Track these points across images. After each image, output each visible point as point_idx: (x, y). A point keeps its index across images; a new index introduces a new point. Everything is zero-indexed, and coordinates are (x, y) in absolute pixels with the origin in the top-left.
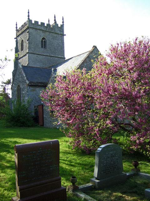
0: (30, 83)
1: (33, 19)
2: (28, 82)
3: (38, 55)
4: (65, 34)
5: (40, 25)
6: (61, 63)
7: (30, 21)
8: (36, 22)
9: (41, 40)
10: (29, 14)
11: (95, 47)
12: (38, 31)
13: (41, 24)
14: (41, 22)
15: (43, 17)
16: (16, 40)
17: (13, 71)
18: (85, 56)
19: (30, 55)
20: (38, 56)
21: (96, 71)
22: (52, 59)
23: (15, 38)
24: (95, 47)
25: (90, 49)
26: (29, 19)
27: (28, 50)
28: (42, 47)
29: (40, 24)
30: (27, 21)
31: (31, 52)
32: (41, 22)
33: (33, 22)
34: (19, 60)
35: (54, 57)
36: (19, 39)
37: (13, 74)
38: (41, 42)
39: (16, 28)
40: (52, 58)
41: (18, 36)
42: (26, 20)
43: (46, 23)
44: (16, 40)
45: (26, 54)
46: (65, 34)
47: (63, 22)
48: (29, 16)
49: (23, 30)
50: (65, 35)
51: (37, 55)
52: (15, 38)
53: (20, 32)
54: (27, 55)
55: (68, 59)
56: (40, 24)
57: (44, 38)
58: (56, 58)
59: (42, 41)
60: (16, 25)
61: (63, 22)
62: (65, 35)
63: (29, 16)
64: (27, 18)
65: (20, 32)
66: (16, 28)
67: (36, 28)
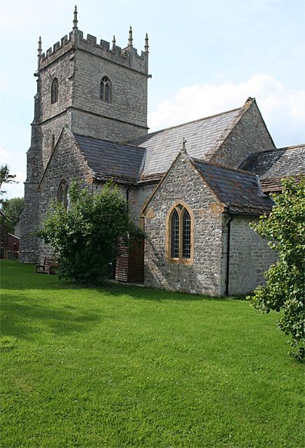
0: (97, 175)
1: (86, 29)
2: (94, 173)
3: (93, 116)
4: (149, 74)
5: (98, 46)
6: (142, 138)
7: (77, 33)
8: (92, 39)
9: (100, 82)
10: (76, 17)
11: (252, 102)
12: (95, 58)
13: (101, 43)
14: (101, 40)
15: (104, 27)
16: (37, 78)
17: (30, 150)
18: (230, 122)
19: (77, 112)
20: (136, 131)
21: (268, 328)
22: (123, 127)
23: (35, 75)
24: (252, 102)
25: (241, 103)
26: (75, 28)
27: (71, 100)
28: (101, 98)
29: (98, 43)
30: (71, 34)
31: (79, 106)
32: (101, 40)
33: (85, 37)
34: (43, 127)
35: (125, 122)
36: (43, 77)
37: (28, 156)
38: (92, 79)
39: (40, 50)
40: (120, 126)
41: (41, 70)
42: (67, 30)
43: (123, 44)
44: (37, 78)
45: (66, 111)
46: (149, 74)
47: (147, 47)
48: (75, 21)
49: (58, 55)
50: (151, 76)
51: (90, 115)
52: (35, 75)
53: (50, 60)
54: (70, 113)
55: (154, 133)
56: (98, 43)
57: (105, 78)
58: (128, 125)
59: (102, 83)
60: (40, 43)
61: (147, 47)
62: (151, 76)
63: (75, 21)
64: (73, 25)
65: (47, 61)
66: (40, 50)
67: (90, 51)
